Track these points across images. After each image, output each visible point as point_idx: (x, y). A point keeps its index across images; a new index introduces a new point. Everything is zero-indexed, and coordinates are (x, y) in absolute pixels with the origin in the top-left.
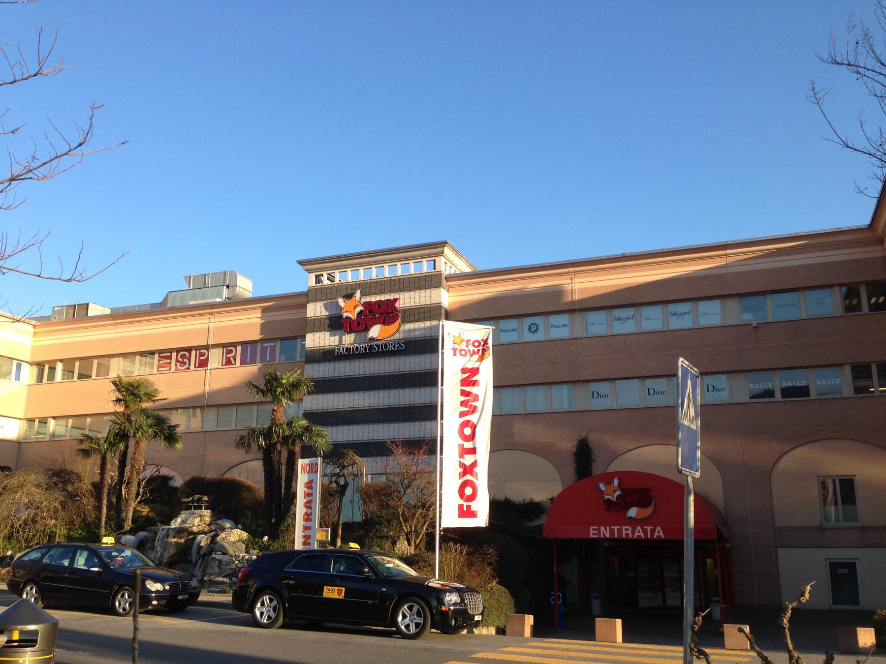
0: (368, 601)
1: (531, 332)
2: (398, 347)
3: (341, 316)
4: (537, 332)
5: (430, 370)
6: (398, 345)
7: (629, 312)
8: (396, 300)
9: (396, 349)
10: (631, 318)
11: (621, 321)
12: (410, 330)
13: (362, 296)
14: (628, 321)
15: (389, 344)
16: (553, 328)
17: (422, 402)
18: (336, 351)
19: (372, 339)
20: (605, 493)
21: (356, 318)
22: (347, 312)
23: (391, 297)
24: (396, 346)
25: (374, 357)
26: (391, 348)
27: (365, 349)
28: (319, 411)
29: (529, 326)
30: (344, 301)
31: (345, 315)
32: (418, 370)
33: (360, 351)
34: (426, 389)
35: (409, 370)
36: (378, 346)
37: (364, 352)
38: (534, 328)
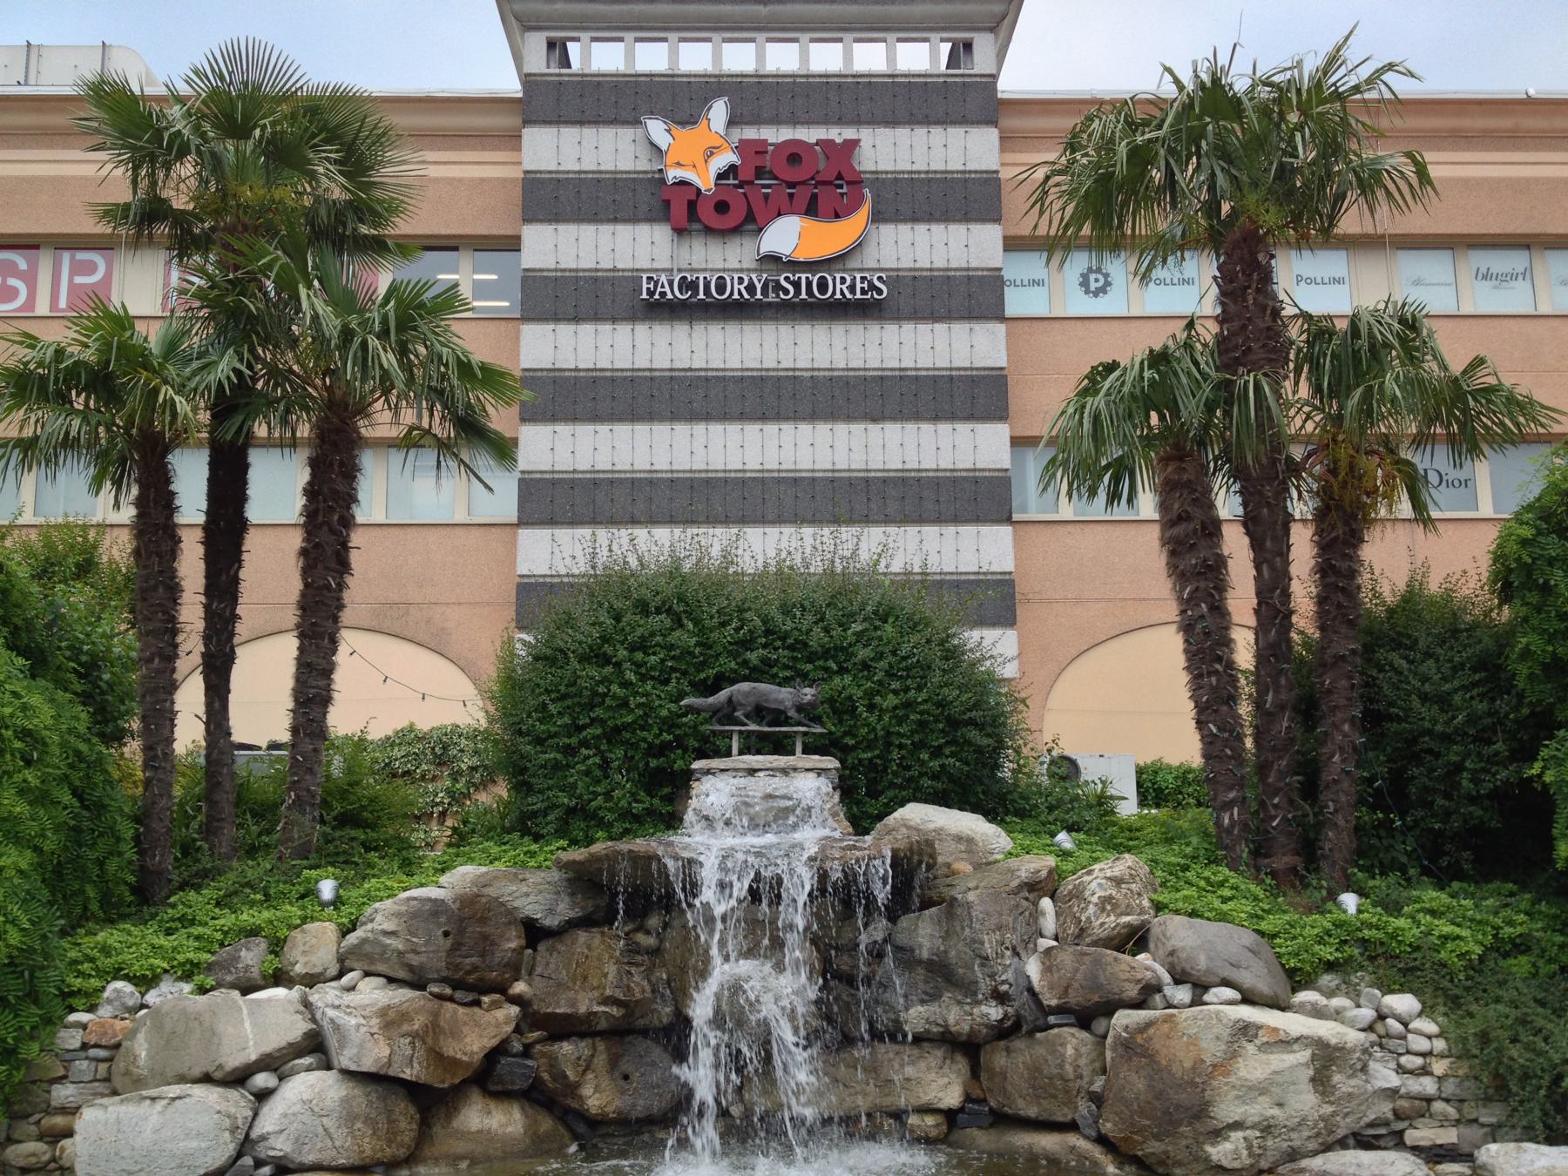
0: (865, 135)
1: (1087, 292)
2: (863, 291)
3: (663, 181)
4: (1105, 292)
5: (965, 369)
6: (865, 285)
7: (1515, 261)
8: (853, 143)
9: (858, 296)
10: (1520, 277)
11: (1494, 282)
12: (361, 740)
13: (732, 122)
14: (1513, 283)
15: (834, 279)
16: (1302, 283)
17: (945, 464)
18: (645, 286)
19: (773, 259)
20: (670, 159)
21: (712, 185)
22: (679, 164)
23: (837, 134)
24: (859, 286)
25: (776, 319)
26: (740, 293)
27: (751, 288)
28: (580, 476)
29: (1082, 275)
30: (668, 131)
31: (673, 174)
32: (928, 369)
33: (732, 293)
34: (955, 426)
35: (897, 365)
36: (797, 285)
37: (746, 296)
38: (1097, 280)
